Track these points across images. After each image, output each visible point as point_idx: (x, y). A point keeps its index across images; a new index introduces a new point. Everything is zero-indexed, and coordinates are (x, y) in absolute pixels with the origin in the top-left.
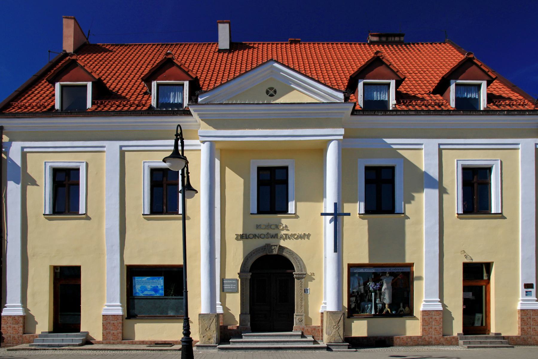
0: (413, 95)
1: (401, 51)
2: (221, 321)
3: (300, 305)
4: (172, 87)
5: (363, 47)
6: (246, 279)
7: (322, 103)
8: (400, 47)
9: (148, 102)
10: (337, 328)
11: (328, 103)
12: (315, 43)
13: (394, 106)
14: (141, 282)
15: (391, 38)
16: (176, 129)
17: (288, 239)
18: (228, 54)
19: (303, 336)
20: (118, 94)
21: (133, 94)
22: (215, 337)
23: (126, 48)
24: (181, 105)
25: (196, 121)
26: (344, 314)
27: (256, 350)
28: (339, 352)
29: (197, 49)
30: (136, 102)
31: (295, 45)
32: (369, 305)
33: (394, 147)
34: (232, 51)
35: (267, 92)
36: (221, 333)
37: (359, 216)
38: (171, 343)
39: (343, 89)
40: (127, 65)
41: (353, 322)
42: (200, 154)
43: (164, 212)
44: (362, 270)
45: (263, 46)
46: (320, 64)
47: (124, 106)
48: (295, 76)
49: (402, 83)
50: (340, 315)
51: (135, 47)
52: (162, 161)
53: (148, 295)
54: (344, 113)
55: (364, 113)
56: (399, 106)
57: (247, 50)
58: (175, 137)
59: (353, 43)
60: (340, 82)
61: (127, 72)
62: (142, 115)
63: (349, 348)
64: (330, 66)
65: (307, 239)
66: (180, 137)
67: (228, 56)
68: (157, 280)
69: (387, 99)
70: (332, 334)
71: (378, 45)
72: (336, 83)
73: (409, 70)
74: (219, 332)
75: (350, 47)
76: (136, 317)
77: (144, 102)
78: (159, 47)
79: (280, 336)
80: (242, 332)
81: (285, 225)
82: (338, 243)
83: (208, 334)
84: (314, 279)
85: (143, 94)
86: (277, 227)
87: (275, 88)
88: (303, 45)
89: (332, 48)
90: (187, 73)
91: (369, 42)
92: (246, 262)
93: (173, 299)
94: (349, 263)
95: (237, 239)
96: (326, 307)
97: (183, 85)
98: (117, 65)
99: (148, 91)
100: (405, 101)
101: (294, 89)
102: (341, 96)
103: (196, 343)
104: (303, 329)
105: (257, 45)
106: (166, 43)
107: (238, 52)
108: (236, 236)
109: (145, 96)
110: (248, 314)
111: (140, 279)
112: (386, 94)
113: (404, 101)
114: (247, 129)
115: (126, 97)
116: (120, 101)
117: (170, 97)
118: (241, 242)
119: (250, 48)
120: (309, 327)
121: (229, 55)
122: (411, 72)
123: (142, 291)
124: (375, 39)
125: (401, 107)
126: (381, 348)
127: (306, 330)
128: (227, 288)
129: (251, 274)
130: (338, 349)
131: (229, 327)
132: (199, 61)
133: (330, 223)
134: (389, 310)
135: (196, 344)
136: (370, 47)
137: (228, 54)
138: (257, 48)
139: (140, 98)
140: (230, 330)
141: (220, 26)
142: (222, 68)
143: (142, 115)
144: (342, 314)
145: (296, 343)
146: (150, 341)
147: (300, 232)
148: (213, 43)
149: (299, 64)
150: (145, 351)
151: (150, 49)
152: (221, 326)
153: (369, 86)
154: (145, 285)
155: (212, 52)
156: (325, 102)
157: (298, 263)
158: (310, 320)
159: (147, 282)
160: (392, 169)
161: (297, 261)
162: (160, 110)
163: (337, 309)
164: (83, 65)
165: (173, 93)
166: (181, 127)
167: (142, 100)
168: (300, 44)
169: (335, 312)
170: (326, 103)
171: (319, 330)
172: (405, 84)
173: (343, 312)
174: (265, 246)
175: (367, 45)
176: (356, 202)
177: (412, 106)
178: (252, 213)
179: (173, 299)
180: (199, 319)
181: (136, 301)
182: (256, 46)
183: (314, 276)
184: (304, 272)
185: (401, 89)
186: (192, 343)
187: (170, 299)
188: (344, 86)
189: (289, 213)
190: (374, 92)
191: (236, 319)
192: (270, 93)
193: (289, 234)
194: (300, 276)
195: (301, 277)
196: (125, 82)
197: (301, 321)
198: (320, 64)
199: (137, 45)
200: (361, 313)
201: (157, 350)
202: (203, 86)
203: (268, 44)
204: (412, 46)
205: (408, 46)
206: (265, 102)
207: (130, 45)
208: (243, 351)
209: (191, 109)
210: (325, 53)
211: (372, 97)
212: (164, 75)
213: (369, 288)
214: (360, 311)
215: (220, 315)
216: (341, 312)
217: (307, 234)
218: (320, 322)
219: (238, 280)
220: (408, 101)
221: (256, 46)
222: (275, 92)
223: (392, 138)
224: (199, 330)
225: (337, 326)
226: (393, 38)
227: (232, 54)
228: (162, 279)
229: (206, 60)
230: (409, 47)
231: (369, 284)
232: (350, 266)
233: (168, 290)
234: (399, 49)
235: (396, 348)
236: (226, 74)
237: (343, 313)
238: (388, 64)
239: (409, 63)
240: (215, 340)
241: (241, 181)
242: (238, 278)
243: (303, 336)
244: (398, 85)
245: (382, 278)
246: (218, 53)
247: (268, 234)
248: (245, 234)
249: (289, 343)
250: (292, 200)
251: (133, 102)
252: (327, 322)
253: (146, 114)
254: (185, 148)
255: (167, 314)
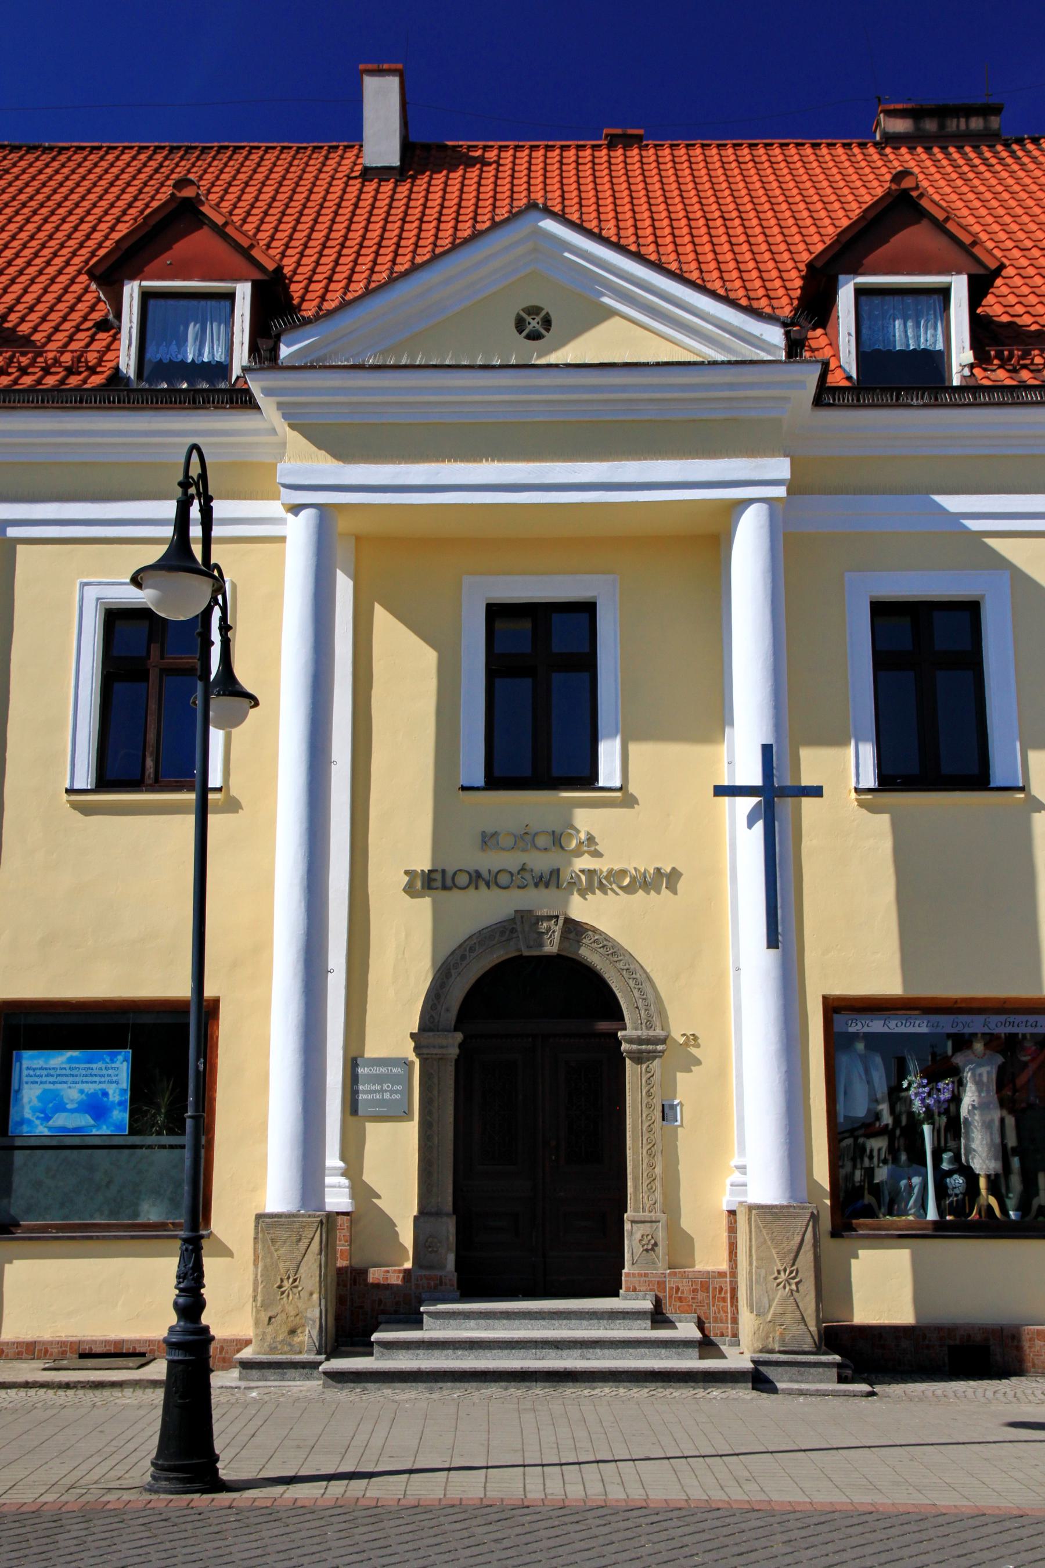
0: (1034, 327)
1: (993, 166)
2: (342, 1246)
3: (645, 1175)
4: (194, 303)
5: (860, 157)
6: (442, 1059)
7: (709, 362)
8: (988, 155)
9: (110, 356)
10: (790, 1284)
11: (729, 363)
12: (694, 145)
13: (967, 372)
14: (44, 1072)
15: (955, 121)
16: (182, 460)
17: (597, 891)
18: (396, 186)
19: (658, 1317)
20: (6, 325)
21: (56, 329)
22: (314, 1322)
23: (46, 158)
24: (223, 369)
25: (273, 431)
26: (814, 1218)
27: (474, 1384)
28: (801, 1399)
29: (291, 165)
30: (67, 358)
31: (625, 150)
32: (916, 1180)
33: (974, 525)
34: (411, 173)
35: (520, 324)
36: (341, 1300)
37: (857, 799)
38: (143, 1350)
39: (786, 312)
40: (46, 221)
41: (857, 1257)
42: (282, 555)
43: (149, 781)
44: (877, 1026)
45: (515, 157)
46: (707, 220)
47: (24, 371)
48: (615, 266)
49: (992, 286)
50: (800, 1223)
51: (78, 157)
52: (128, 580)
53: (69, 1130)
54: (786, 399)
55: (858, 400)
56: (985, 370)
57: (460, 172)
58: (179, 491)
59: (824, 141)
60: (778, 283)
61: (43, 246)
62: (84, 404)
63: (841, 1380)
64: (743, 225)
65: (668, 892)
66: (198, 489)
67: (394, 192)
68: (104, 1066)
69: (940, 346)
70: (771, 1312)
71: (912, 149)
72: (764, 287)
73: (1021, 235)
74: (334, 1300)
75: (812, 158)
76: (12, 1229)
77: (92, 358)
78: (159, 157)
79: (570, 1319)
80: (424, 1296)
81: (588, 833)
82: (782, 907)
83: (291, 1305)
84: (698, 1062)
85: (94, 330)
86: (557, 840)
87: (548, 308)
88: (652, 151)
89: (753, 160)
90: (246, 253)
91: (878, 138)
92: (442, 985)
93: (163, 1147)
94: (827, 992)
95: (410, 890)
96: (745, 1185)
97: (231, 296)
98: (28, 221)
99: (111, 317)
100: (1006, 353)
101: (611, 313)
102: (775, 335)
103: (239, 1351)
104: (661, 1285)
105: (495, 152)
106: (186, 144)
107: (431, 178)
108: (406, 879)
109: (100, 336)
110: (447, 1215)
111: (39, 1063)
112: (935, 329)
113: (1002, 352)
114: (449, 461)
115: (33, 338)
116: (9, 354)
117: (186, 340)
118: (425, 904)
119: (470, 162)
120: (684, 1275)
121: (399, 189)
122: (1029, 244)
123: (43, 1111)
124: (900, 126)
125: (992, 375)
126: (972, 1383)
127: (671, 1289)
128: (370, 1097)
129: (459, 1037)
130: (797, 1382)
131: (375, 1275)
132: (296, 206)
133: (750, 825)
134: (993, 1201)
135: (238, 1356)
136: (881, 155)
137: (396, 186)
138: (495, 162)
139: (82, 344)
140: (377, 1286)
141: (372, 85)
142: (374, 235)
143: (84, 404)
144: (808, 1217)
145: (631, 1351)
146: (58, 1342)
147: (642, 863)
148: (346, 144)
149: (636, 220)
150: (32, 1392)
151: (128, 165)
152: (340, 1271)
153: (877, 300)
154: (58, 1086)
155: (341, 179)
156: (720, 357)
157: (635, 992)
158: (688, 1242)
159: (67, 1076)
160: (971, 610)
161: (632, 983)
162: (147, 386)
163: (787, 1195)
164: (220, 221)
165: (198, 326)
166: (204, 450)
167: (86, 352)
168: (640, 148)
169: (782, 1207)
170: (723, 363)
171: (721, 1289)
172: (1005, 290)
173: (811, 1208)
174: (513, 920)
175: (871, 150)
176: (840, 741)
177: (1032, 371)
178: (466, 784)
179: (163, 1147)
180: (255, 1238)
181: (19, 1157)
182: (491, 155)
183: (698, 1046)
184: (659, 1032)
185: (992, 306)
186: (207, 1351)
187: (150, 1147)
188: (791, 299)
189: (601, 784)
190: (894, 321)
191: (401, 1240)
192: (531, 326)
193: (601, 872)
194: (644, 1047)
195: (649, 1052)
196: (33, 281)
197: (653, 1249)
198: (707, 220)
199: (83, 148)
200: (884, 1216)
201: (83, 1387)
202: (303, 299)
203: (533, 148)
204: (1030, 147)
205: (1015, 147)
206: (513, 362)
207: (62, 150)
208: (421, 1386)
209: (255, 386)
210: (727, 181)
211: (889, 339)
212: (166, 259)
213: (911, 1102)
214: (880, 1208)
215: (340, 1218)
216: (802, 1208)
217: (668, 870)
218: (725, 1254)
219: (408, 1064)
220: (1016, 352)
221: (491, 155)
222: (547, 323)
223: (963, 493)
224: (255, 1290)
225: (791, 1272)
226: (963, 121)
227: (408, 186)
228: (125, 1060)
229: (317, 208)
230: (1020, 154)
231: (910, 1085)
232: (833, 1007)
233: (145, 1108)
234: (985, 161)
235: (1034, 1385)
236: (385, 259)
237: (812, 1213)
238: (941, 216)
239: (1019, 211)
240: (315, 1333)
241: (429, 657)
242: (412, 1057)
243: (659, 1317)
244: (978, 289)
245: (959, 1059)
246: (360, 180)
247: (523, 869)
248: (440, 869)
249: (606, 1351)
250: (612, 736)
251: (56, 356)
252: (751, 1256)
253: (95, 402)
254: (217, 531)
255: (136, 1215)
